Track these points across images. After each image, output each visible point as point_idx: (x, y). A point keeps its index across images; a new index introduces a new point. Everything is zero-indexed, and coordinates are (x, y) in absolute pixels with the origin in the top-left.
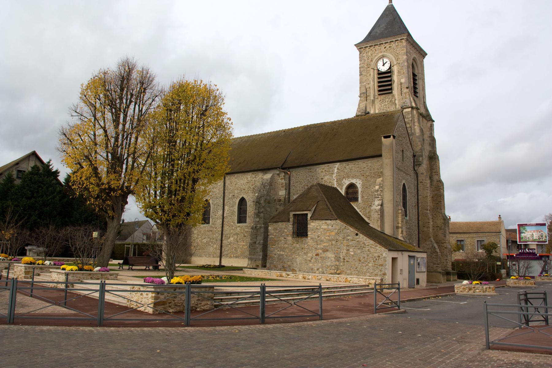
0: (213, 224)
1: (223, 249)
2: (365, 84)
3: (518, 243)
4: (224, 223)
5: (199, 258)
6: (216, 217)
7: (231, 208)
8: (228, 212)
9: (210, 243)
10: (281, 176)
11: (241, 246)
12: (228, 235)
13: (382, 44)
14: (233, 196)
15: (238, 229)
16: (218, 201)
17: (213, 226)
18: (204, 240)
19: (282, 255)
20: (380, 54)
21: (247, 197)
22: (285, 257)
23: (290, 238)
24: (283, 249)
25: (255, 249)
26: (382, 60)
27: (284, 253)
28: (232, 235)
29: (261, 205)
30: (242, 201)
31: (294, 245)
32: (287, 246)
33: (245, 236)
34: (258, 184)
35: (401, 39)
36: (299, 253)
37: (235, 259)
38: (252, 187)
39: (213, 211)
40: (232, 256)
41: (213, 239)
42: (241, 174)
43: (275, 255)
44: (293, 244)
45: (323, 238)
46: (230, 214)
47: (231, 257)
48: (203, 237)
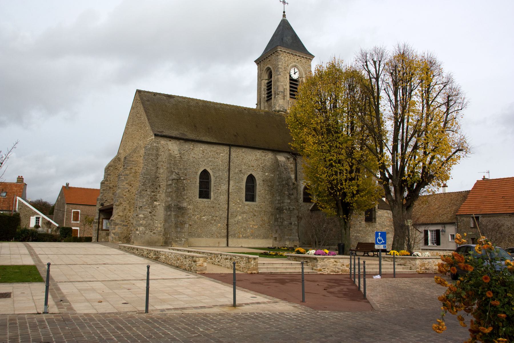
0: (215, 199)
1: (229, 229)
2: (282, 84)
3: (73, 210)
4: (230, 199)
5: (197, 239)
6: (219, 191)
7: (237, 184)
8: (234, 188)
9: (213, 222)
10: (290, 160)
11: (251, 226)
12: (235, 213)
13: (296, 55)
14: (240, 171)
15: (246, 207)
16: (221, 174)
17: (216, 202)
18: (203, 217)
19: (359, 236)
20: (294, 64)
21: (257, 175)
22: (361, 238)
23: (363, 222)
24: (358, 232)
25: (291, 230)
26: (294, 68)
27: (360, 235)
28: (239, 213)
29: (289, 187)
30: (251, 179)
31: (367, 228)
32: (362, 228)
33: (255, 215)
34: (268, 164)
35: (309, 59)
36: (370, 235)
37: (244, 240)
38: (262, 165)
39: (215, 185)
40: (241, 236)
41: (216, 217)
42: (250, 150)
43: (353, 236)
44: (366, 228)
45: (386, 223)
46: (235, 190)
47: (239, 237)
48: (203, 214)
